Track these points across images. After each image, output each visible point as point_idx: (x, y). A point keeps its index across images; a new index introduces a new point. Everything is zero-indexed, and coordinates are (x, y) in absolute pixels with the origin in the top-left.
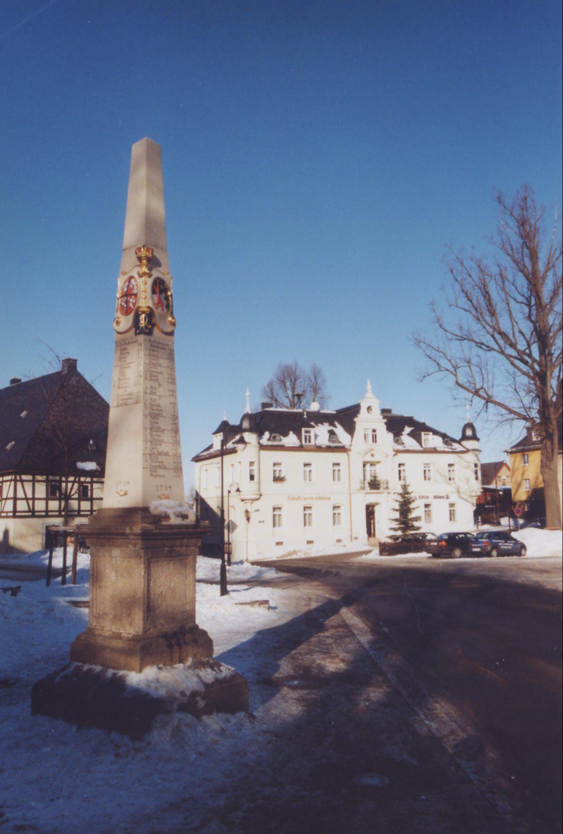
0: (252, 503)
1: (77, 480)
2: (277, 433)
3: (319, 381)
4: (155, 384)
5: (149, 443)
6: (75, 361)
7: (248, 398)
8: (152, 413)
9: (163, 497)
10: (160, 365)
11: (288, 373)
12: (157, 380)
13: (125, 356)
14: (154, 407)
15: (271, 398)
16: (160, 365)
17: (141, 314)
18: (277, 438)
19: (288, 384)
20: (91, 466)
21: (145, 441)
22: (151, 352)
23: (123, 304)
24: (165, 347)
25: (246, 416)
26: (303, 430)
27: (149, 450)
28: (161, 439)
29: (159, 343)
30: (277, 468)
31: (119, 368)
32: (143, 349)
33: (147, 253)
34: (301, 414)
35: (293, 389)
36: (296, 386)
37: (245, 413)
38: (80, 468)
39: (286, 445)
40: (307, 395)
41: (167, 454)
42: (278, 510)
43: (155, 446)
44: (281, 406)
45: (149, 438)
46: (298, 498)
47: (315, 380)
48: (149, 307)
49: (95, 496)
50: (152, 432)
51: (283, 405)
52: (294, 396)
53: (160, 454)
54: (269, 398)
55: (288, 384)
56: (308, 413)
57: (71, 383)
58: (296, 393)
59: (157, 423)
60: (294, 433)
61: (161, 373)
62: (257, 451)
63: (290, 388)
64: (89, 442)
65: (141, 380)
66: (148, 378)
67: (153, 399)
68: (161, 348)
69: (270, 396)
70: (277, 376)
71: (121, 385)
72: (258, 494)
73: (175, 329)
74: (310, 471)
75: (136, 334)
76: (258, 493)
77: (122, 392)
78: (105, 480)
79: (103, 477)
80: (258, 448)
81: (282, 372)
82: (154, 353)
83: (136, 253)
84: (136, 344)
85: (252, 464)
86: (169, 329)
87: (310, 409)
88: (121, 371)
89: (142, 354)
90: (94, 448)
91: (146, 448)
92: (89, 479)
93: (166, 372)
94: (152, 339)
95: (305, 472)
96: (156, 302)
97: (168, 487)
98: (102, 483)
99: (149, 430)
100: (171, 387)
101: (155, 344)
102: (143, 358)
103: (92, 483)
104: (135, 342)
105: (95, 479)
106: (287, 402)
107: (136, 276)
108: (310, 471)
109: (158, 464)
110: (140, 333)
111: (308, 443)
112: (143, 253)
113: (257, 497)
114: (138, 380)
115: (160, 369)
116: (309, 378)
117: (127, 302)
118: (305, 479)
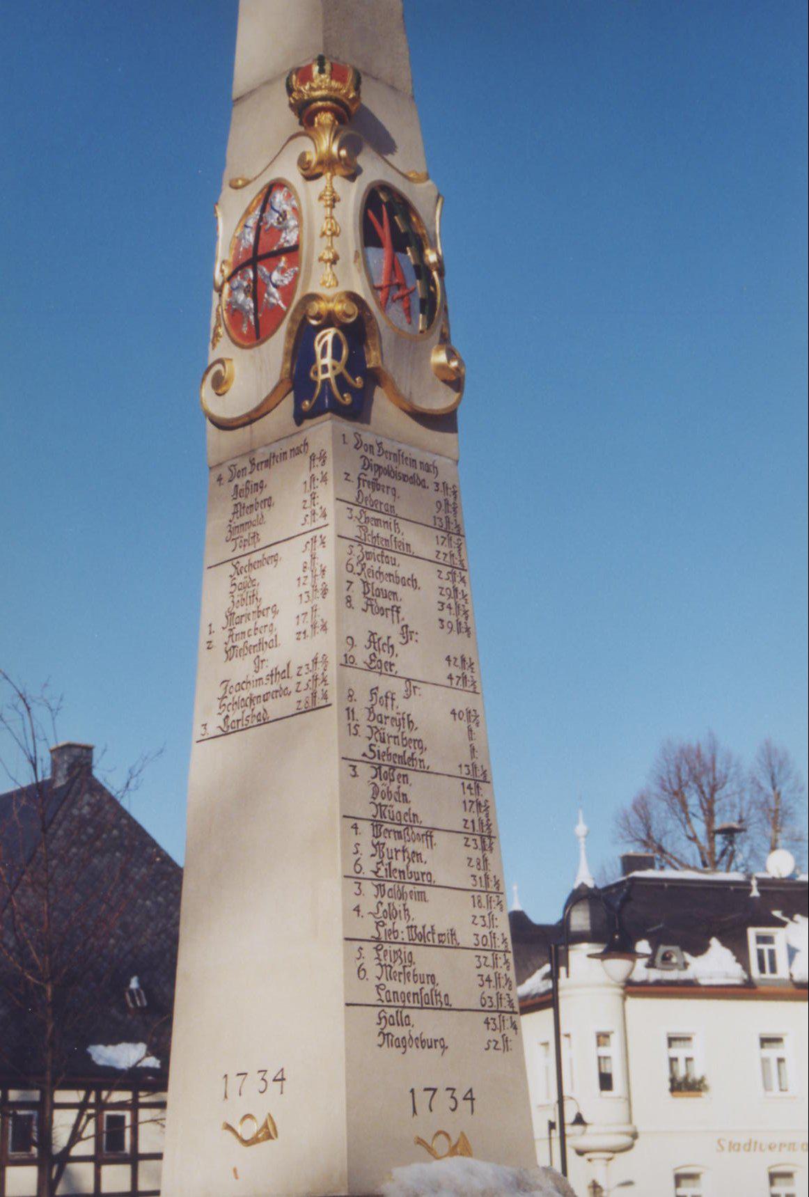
0: (610, 1159)
1: (92, 1099)
2: (673, 944)
3: (784, 789)
4: (385, 627)
5: (369, 888)
6: (89, 749)
7: (582, 840)
8: (379, 755)
9: (441, 1145)
10: (406, 549)
11: (691, 770)
12: (397, 610)
13: (253, 516)
14: (390, 730)
15: (645, 844)
16: (406, 549)
17: (318, 329)
18: (674, 960)
19: (693, 800)
20: (127, 1055)
21: (355, 877)
22: (366, 491)
23: (241, 297)
24: (423, 475)
25: (579, 896)
26: (752, 932)
27: (371, 921)
28: (421, 868)
29: (398, 456)
30: (680, 1052)
31: (229, 569)
32: (330, 477)
33: (335, 84)
34: (743, 887)
35: (710, 814)
36: (716, 807)
37: (576, 886)
38: (101, 1062)
39: (703, 982)
40: (753, 830)
41: (448, 941)
42: (690, 1182)
43: (398, 904)
44: (676, 865)
45: (368, 865)
46: (751, 1146)
47: (774, 788)
48: (353, 297)
49: (143, 1148)
50: (382, 840)
51: (681, 864)
52: (711, 834)
53: (421, 937)
54: (638, 844)
55: (693, 800)
56: (761, 882)
57: (75, 812)
58: (718, 825)
59: (405, 798)
60: (725, 943)
61: (413, 582)
62: (619, 1000)
63: (700, 813)
64: (128, 983)
65: (328, 608)
66: (359, 600)
67: (381, 693)
68: (404, 478)
69: (643, 836)
70: (661, 778)
71: (240, 644)
72: (626, 1133)
73: (459, 401)
74: (780, 1060)
75: (300, 417)
76: (628, 1128)
77: (242, 668)
78: (170, 1096)
79: (164, 1087)
80: (621, 991)
81: (672, 768)
82: (377, 495)
83: (290, 90)
84: (303, 460)
85: (603, 1038)
86: (440, 400)
87: (765, 870)
88: (240, 579)
89: (327, 496)
90: (142, 1002)
91: (357, 909)
92: (126, 1096)
93: (429, 578)
94: (368, 438)
95: (765, 1061)
96: (381, 281)
97: (459, 1095)
98: (162, 1105)
99: (366, 828)
100: (457, 644)
101: (382, 461)
102: (331, 518)
103: (135, 1106)
104: (296, 452)
105: (144, 1098)
106: (690, 853)
107: (293, 175)
108: (780, 1060)
109: (412, 987)
110: (315, 413)
111: (768, 975)
112: (321, 84)
113: (626, 1140)
114: (314, 609)
115: (405, 567)
116: (754, 780)
117: (256, 291)
118: (767, 1087)
